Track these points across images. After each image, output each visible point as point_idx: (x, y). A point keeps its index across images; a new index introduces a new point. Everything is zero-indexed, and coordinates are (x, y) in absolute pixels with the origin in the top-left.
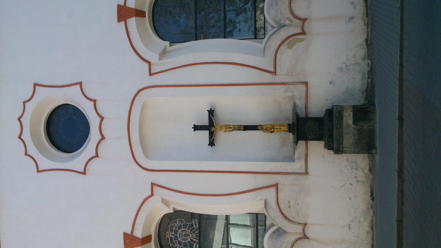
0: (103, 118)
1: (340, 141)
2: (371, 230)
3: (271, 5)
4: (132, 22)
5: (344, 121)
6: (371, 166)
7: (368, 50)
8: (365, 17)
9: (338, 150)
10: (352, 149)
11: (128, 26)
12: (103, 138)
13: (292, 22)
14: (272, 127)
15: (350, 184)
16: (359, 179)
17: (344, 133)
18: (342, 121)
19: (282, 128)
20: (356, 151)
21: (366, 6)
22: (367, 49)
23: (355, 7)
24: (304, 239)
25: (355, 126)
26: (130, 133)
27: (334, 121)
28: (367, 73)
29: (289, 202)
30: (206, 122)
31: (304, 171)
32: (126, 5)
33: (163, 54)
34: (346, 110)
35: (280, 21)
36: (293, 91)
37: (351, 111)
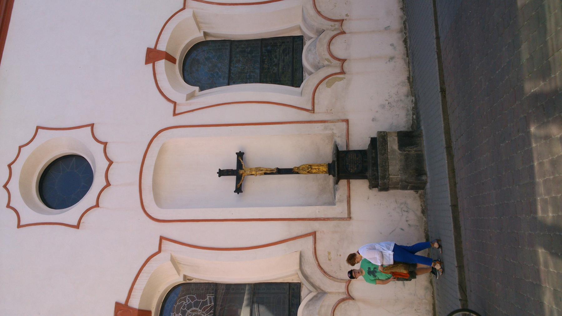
0: (110, 185)
1: (386, 167)
2: (429, 285)
3: (310, 50)
4: (161, 64)
5: (388, 147)
6: (424, 207)
7: (411, 88)
8: (406, 57)
9: (385, 188)
10: (400, 176)
11: (155, 68)
12: (108, 184)
13: (331, 63)
14: (310, 167)
15: (402, 229)
16: (410, 222)
17: (389, 159)
18: (386, 146)
19: (321, 168)
20: (404, 178)
21: (406, 47)
22: (410, 86)
23: (395, 48)
24: (347, 301)
25: (401, 151)
26: (143, 177)
27: (378, 146)
28: (411, 109)
29: (329, 253)
30: (233, 166)
31: (346, 216)
32: (156, 49)
33: (191, 96)
34: (390, 135)
35: (319, 63)
36: (333, 129)
37: (396, 136)
